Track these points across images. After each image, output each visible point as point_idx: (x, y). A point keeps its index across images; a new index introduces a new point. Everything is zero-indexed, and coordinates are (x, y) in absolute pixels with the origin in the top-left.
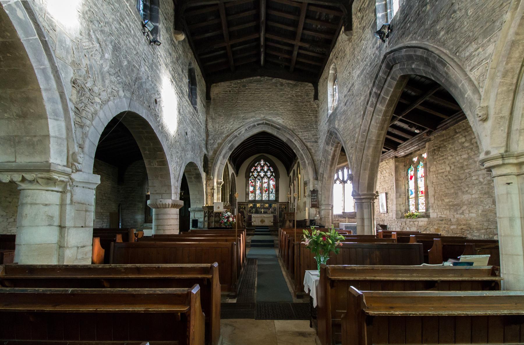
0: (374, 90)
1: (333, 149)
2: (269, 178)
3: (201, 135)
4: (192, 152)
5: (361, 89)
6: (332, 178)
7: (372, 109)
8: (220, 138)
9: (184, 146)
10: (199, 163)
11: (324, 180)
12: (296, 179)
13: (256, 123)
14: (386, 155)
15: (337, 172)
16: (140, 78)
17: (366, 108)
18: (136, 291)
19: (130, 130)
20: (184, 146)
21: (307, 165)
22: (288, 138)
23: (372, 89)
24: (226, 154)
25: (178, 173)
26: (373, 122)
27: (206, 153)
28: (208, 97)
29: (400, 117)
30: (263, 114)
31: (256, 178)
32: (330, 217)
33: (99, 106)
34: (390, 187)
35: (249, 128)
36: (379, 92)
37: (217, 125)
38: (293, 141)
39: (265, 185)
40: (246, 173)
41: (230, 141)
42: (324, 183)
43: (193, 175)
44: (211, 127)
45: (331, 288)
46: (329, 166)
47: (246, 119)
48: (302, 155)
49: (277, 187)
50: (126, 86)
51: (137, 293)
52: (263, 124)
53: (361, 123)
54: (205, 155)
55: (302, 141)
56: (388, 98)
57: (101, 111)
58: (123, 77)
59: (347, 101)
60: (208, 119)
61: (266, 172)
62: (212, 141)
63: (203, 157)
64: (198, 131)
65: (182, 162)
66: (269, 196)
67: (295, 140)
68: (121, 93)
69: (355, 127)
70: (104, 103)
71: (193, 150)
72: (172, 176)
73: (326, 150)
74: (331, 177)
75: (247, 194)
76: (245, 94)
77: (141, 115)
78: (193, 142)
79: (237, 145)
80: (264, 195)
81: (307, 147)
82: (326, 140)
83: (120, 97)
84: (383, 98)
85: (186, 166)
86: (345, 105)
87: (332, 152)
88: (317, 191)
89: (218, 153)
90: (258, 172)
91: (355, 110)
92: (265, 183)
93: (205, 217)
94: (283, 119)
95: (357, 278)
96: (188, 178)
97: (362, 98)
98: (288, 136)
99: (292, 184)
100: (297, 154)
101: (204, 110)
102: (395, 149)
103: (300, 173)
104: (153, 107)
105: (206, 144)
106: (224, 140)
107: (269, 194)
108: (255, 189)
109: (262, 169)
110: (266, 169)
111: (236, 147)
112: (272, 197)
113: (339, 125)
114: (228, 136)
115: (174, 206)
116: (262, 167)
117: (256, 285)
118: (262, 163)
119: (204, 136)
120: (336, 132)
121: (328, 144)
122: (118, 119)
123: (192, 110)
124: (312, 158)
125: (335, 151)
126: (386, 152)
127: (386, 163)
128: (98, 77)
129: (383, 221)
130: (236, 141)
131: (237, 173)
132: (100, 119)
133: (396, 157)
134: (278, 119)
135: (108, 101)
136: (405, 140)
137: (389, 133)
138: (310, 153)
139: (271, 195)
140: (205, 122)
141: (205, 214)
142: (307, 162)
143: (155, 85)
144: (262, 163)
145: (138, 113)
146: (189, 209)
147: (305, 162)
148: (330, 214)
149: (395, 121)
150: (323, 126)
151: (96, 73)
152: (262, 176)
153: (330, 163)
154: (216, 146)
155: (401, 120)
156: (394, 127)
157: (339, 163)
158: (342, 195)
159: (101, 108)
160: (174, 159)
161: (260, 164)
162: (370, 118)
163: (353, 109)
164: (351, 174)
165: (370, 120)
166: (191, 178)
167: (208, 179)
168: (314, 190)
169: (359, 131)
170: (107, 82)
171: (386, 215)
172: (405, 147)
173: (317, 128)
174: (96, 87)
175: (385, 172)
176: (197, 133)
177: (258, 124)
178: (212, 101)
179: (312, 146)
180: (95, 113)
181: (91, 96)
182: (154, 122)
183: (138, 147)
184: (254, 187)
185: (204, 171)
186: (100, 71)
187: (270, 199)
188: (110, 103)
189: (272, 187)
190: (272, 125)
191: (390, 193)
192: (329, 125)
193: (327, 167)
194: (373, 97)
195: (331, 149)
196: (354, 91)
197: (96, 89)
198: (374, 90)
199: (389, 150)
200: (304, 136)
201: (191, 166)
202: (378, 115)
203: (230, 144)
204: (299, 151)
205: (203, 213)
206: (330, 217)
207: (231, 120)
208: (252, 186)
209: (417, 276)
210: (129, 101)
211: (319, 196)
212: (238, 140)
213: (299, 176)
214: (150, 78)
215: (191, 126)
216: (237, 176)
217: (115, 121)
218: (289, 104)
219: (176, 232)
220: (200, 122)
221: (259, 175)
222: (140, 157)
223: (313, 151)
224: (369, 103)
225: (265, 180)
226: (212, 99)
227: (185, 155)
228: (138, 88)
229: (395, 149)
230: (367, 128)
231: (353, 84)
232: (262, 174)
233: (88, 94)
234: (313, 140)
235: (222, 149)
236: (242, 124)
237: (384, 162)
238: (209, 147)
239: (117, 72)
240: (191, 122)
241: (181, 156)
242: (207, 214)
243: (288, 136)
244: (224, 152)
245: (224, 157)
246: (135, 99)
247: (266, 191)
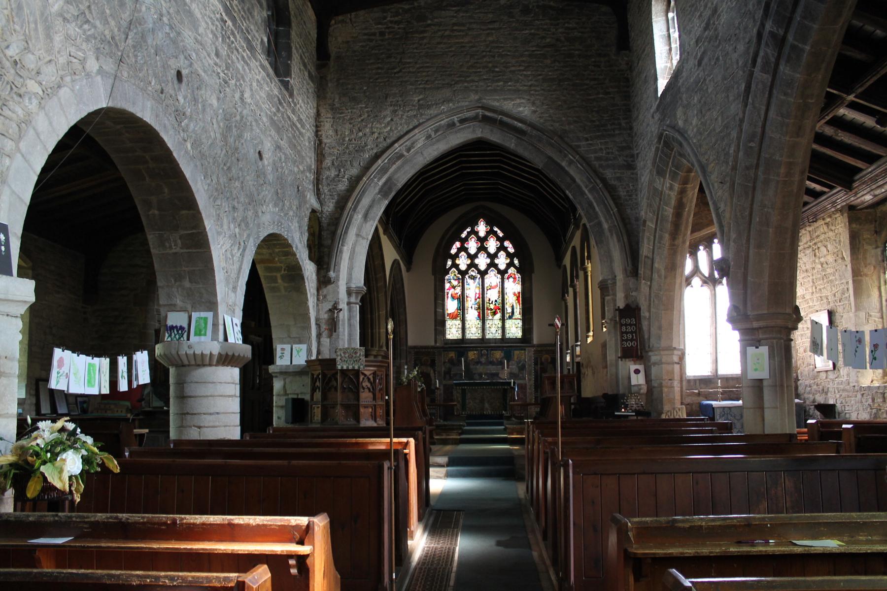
0: (769, 26)
1: (677, 186)
2: (502, 273)
3: (302, 157)
4: (276, 205)
5: (737, 22)
6: (678, 271)
7: (767, 78)
8: (356, 164)
9: (253, 189)
10: (297, 236)
11: (655, 276)
12: (581, 273)
13: (455, 119)
14: (825, 203)
15: (694, 253)
16: (140, 22)
17: (751, 74)
18: (113, 576)
19: (113, 156)
20: (253, 189)
21: (607, 233)
22: (550, 158)
23: (763, 25)
24: (371, 207)
25: (236, 266)
26: (772, 114)
27: (316, 206)
28: (322, 53)
29: (851, 97)
30: (476, 92)
31: (463, 273)
32: (676, 384)
33: (35, 102)
34: (838, 295)
35: (436, 131)
36: (781, 32)
37: (348, 126)
38: (564, 164)
39: (493, 295)
40: (434, 261)
41: (384, 170)
42: (655, 285)
43: (278, 270)
44: (331, 132)
45: (636, 580)
46: (667, 236)
47: (429, 107)
48: (590, 205)
49: (526, 298)
50: (106, 46)
51: (113, 581)
52: (475, 118)
53: (741, 115)
54: (314, 211)
55: (589, 164)
56: (808, 48)
57: (42, 115)
58: (98, 23)
59: (704, 53)
60: (323, 111)
61: (472, 257)
62: (333, 173)
63: (306, 220)
64: (293, 146)
65: (249, 236)
66: (503, 328)
67: (571, 162)
68: (93, 65)
69: (726, 127)
70: (49, 92)
71: (279, 199)
72: (219, 276)
73: (656, 189)
74: (674, 266)
75: (440, 324)
76: (423, 38)
77: (139, 115)
78: (280, 179)
79: (402, 179)
80: (488, 323)
81: (604, 181)
82: (654, 163)
83: (88, 75)
84: (794, 47)
85: (260, 247)
86: (700, 64)
87: (674, 195)
88: (638, 309)
89: (350, 204)
90: (472, 257)
91: (724, 78)
92: (491, 288)
93: (313, 390)
94: (534, 104)
95: (705, 551)
96: (266, 277)
97: (741, 48)
98: (550, 152)
99: (571, 290)
100: (575, 202)
101: (311, 87)
102: (848, 185)
103: (589, 258)
104: (172, 92)
105: (317, 182)
106: (366, 169)
107: (503, 320)
108: (462, 308)
109: (482, 248)
110: (492, 245)
111: (400, 185)
112: (515, 329)
113: (686, 121)
114: (377, 157)
115: (226, 359)
116: (482, 241)
117: (452, 583)
118: (482, 228)
119: (310, 158)
120: (680, 138)
121: (661, 173)
122: (84, 128)
123: (276, 92)
124: (619, 211)
125: (682, 192)
126: (822, 193)
127: (827, 224)
128: (36, 29)
129: (825, 392)
130: (399, 168)
131: (409, 263)
132: (38, 134)
133: (851, 208)
134: (519, 105)
135: (59, 87)
136: (871, 159)
137: (820, 138)
138: (614, 200)
139: (509, 323)
140: (312, 121)
141: (314, 381)
142: (606, 226)
143: (179, 34)
144: (482, 228)
145: (131, 109)
146: (271, 368)
147: (600, 224)
148: (677, 377)
149: (838, 107)
150: (649, 125)
151: (31, 19)
152: (483, 267)
153: (669, 226)
154: (342, 186)
155: (853, 106)
156: (839, 123)
157: (696, 228)
158: (708, 321)
159: (41, 106)
160: (225, 227)
161: (476, 233)
162: (765, 101)
163: (719, 78)
164: (722, 260)
165: (764, 108)
166: (274, 280)
167: (324, 281)
168: (628, 306)
169: (739, 138)
170: (58, 38)
171: (831, 376)
172: (874, 180)
173: (631, 128)
174: (30, 56)
175: (823, 249)
176: (289, 151)
177: (462, 121)
178: (332, 63)
179: (619, 179)
180: (27, 121)
181: (18, 78)
182: (171, 132)
183: (130, 198)
184: (462, 300)
185: (310, 259)
186: (42, 14)
187: (507, 336)
188: (64, 92)
189: (511, 300)
190: (502, 123)
191: (840, 310)
192: (662, 120)
193: (661, 238)
194: (767, 44)
195: (671, 188)
196: (720, 28)
197: (30, 61)
198: (769, 26)
199: (831, 188)
200: (595, 152)
201: (274, 245)
202: (785, 94)
203: (384, 180)
204: (583, 194)
205: (307, 380)
206: (676, 384)
207: (388, 112)
208: (453, 298)
209: (868, 542)
210: (111, 81)
211: (645, 324)
212: (407, 168)
213: (589, 266)
214: (165, 19)
215: (273, 133)
216: (408, 270)
217: (75, 131)
218: (548, 61)
219: (235, 434)
220: (300, 120)
221: (472, 265)
222: (135, 226)
223: (622, 193)
224: (759, 60)
225: (492, 278)
226: (333, 55)
227: (257, 216)
228: (134, 47)
229: (848, 185)
230: (759, 130)
231: (715, 11)
232: (482, 261)
233: (10, 75)
234: (621, 161)
235: (363, 193)
236: (415, 122)
237: (821, 222)
238: (325, 189)
239: (83, 13)
240: (273, 122)
241: (244, 219)
242: (318, 384)
243: (550, 152)
244: (365, 202)
245: (366, 216)
246: (125, 74)
247: (495, 313)
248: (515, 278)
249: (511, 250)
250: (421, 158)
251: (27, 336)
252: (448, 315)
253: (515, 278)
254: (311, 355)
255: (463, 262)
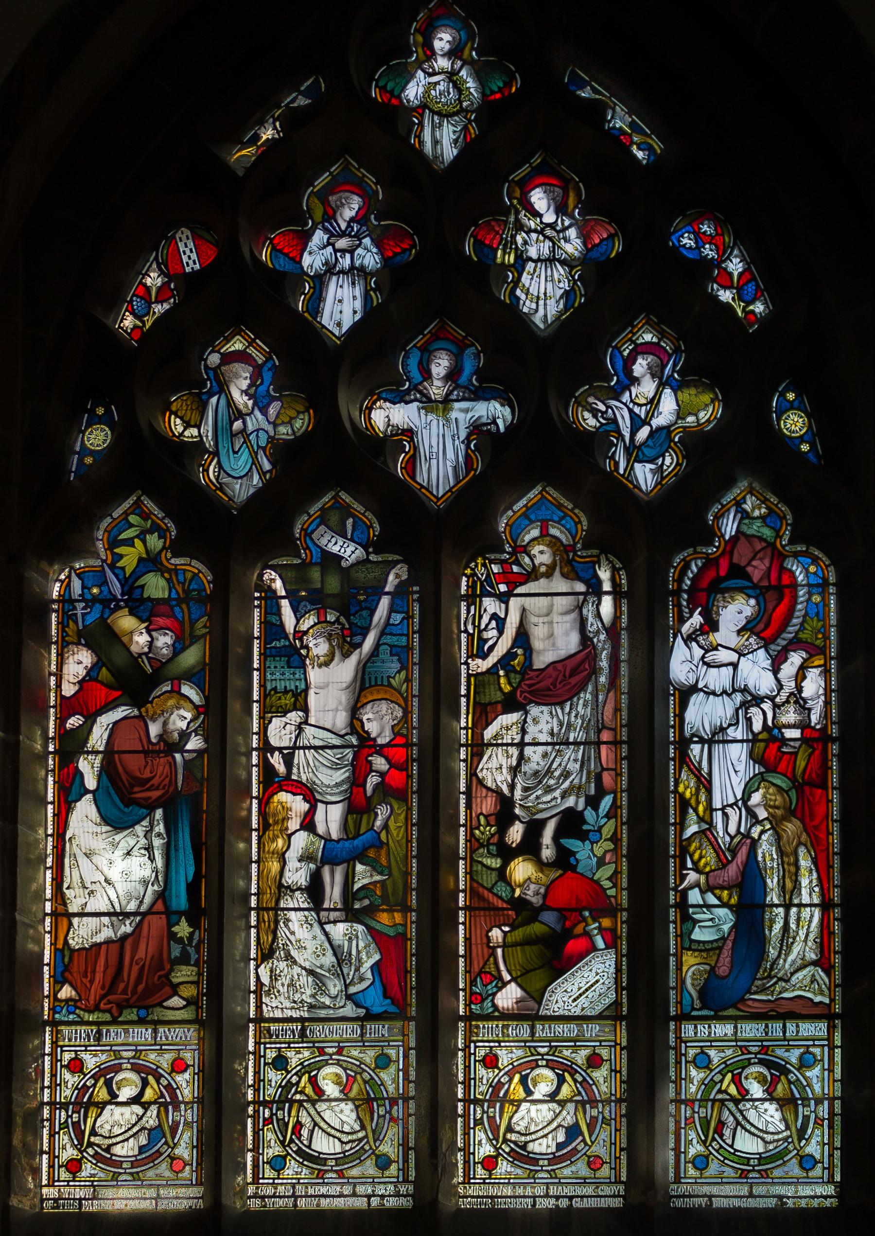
39: (529, 757)
107: (645, 1014)
109: (441, 289)
184: (199, 809)
221: (331, 460)
247: (554, 957)
248: (775, 594)
249: (735, 288)
250: (180, 429)
251: (657, 1125)
252: (72, 963)
253: (775, 594)
254: (680, 1094)
255: (237, 425)
